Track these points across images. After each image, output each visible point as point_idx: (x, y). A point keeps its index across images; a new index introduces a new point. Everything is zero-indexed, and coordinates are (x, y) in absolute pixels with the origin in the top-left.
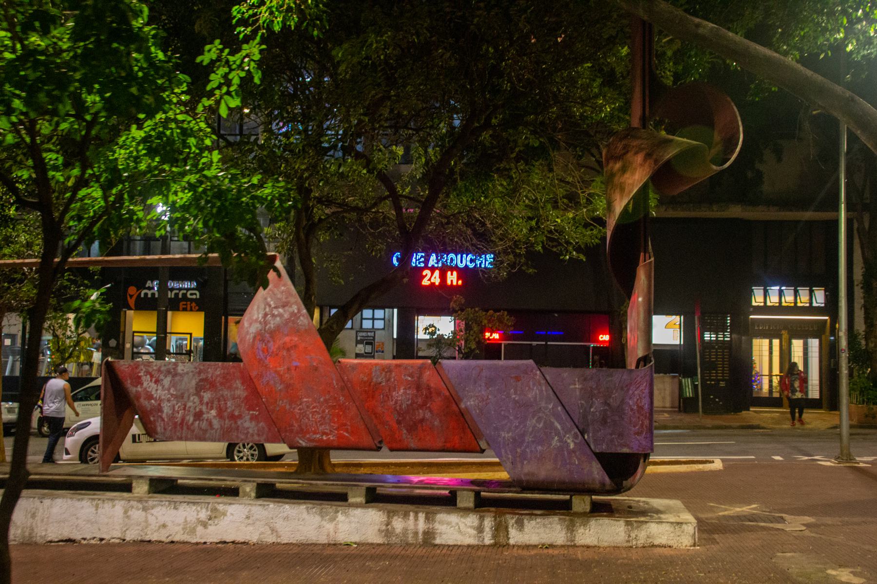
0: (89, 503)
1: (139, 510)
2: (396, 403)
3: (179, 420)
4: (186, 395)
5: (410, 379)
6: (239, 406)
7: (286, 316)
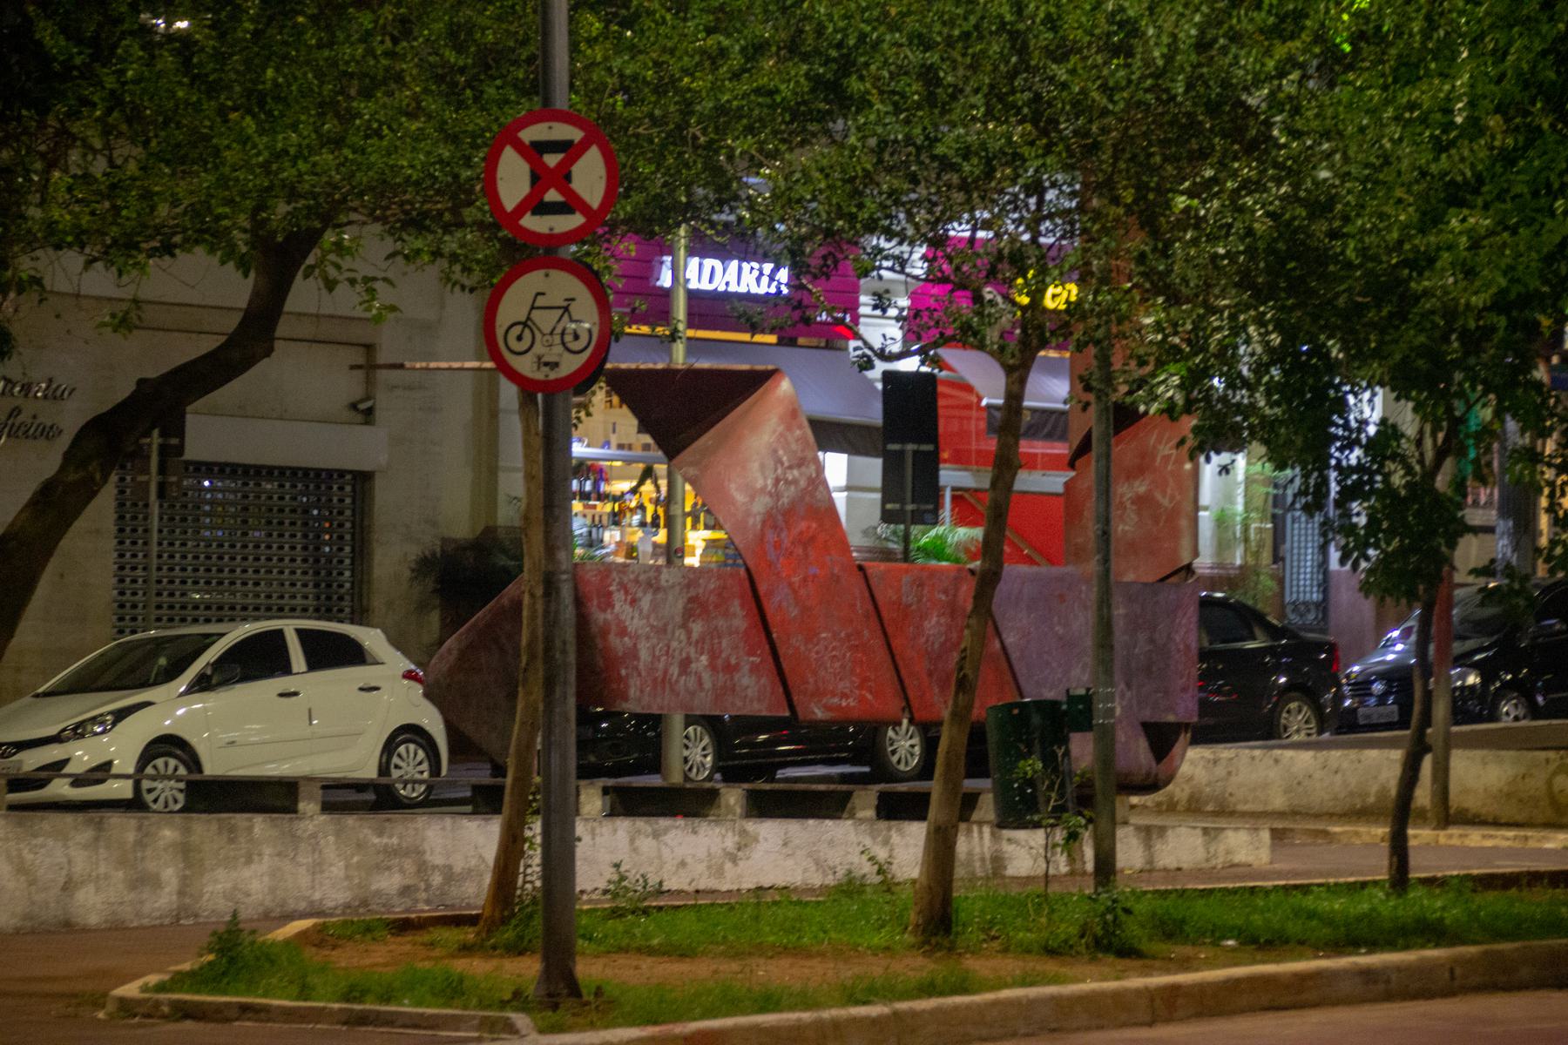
3: (659, 674)
4: (670, 628)
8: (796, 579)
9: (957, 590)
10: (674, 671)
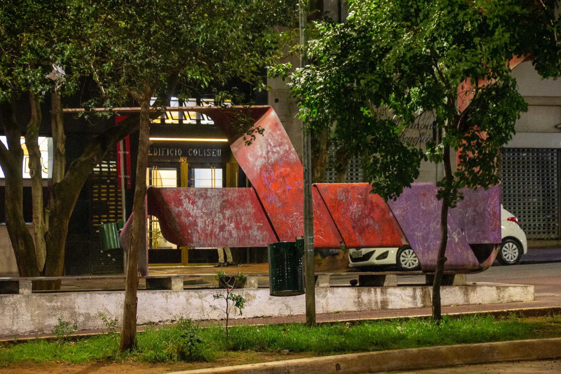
0: (160, 295)
1: (196, 298)
2: (352, 214)
4: (213, 213)
5: (360, 197)
6: (250, 220)
7: (282, 153)
8: (279, 192)
10: (217, 230)
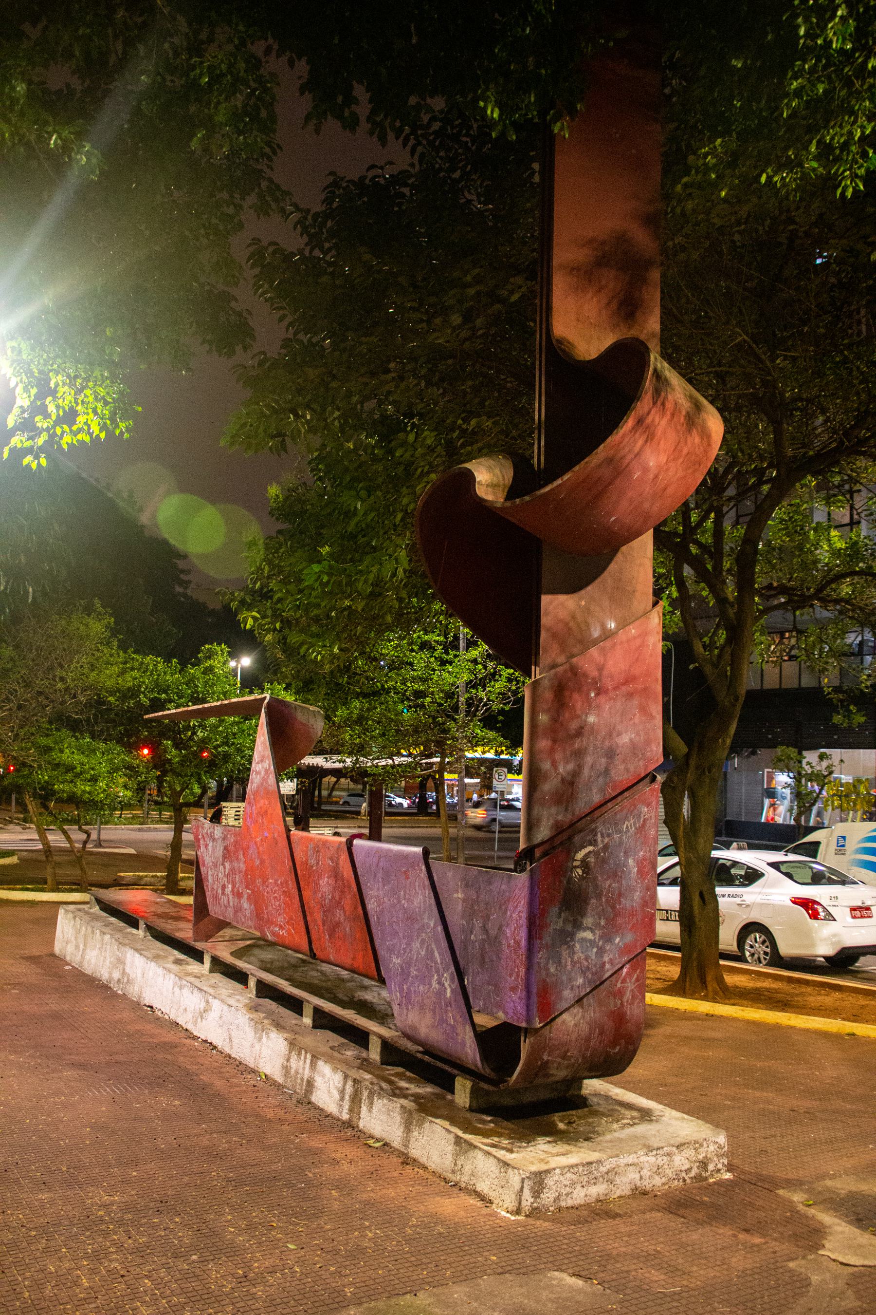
9: (338, 858)
